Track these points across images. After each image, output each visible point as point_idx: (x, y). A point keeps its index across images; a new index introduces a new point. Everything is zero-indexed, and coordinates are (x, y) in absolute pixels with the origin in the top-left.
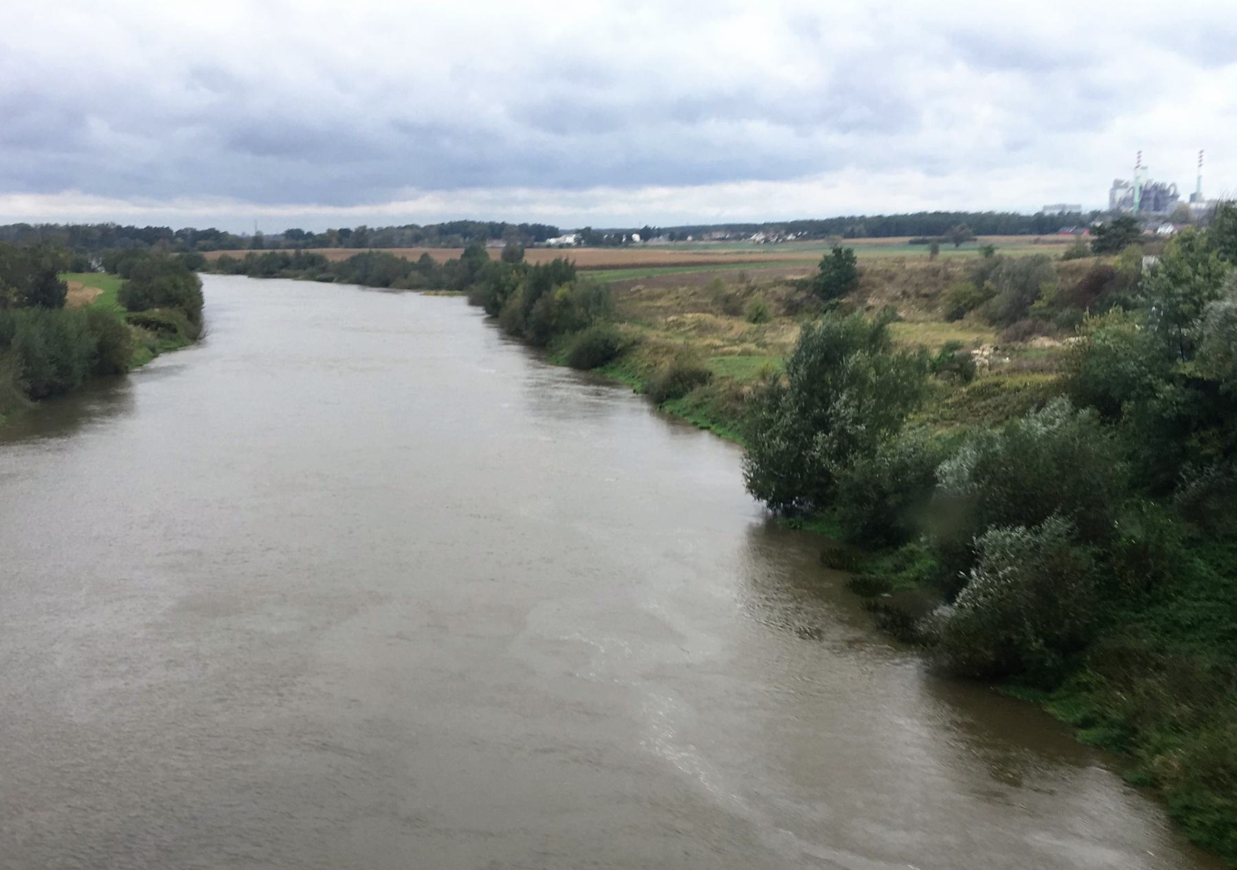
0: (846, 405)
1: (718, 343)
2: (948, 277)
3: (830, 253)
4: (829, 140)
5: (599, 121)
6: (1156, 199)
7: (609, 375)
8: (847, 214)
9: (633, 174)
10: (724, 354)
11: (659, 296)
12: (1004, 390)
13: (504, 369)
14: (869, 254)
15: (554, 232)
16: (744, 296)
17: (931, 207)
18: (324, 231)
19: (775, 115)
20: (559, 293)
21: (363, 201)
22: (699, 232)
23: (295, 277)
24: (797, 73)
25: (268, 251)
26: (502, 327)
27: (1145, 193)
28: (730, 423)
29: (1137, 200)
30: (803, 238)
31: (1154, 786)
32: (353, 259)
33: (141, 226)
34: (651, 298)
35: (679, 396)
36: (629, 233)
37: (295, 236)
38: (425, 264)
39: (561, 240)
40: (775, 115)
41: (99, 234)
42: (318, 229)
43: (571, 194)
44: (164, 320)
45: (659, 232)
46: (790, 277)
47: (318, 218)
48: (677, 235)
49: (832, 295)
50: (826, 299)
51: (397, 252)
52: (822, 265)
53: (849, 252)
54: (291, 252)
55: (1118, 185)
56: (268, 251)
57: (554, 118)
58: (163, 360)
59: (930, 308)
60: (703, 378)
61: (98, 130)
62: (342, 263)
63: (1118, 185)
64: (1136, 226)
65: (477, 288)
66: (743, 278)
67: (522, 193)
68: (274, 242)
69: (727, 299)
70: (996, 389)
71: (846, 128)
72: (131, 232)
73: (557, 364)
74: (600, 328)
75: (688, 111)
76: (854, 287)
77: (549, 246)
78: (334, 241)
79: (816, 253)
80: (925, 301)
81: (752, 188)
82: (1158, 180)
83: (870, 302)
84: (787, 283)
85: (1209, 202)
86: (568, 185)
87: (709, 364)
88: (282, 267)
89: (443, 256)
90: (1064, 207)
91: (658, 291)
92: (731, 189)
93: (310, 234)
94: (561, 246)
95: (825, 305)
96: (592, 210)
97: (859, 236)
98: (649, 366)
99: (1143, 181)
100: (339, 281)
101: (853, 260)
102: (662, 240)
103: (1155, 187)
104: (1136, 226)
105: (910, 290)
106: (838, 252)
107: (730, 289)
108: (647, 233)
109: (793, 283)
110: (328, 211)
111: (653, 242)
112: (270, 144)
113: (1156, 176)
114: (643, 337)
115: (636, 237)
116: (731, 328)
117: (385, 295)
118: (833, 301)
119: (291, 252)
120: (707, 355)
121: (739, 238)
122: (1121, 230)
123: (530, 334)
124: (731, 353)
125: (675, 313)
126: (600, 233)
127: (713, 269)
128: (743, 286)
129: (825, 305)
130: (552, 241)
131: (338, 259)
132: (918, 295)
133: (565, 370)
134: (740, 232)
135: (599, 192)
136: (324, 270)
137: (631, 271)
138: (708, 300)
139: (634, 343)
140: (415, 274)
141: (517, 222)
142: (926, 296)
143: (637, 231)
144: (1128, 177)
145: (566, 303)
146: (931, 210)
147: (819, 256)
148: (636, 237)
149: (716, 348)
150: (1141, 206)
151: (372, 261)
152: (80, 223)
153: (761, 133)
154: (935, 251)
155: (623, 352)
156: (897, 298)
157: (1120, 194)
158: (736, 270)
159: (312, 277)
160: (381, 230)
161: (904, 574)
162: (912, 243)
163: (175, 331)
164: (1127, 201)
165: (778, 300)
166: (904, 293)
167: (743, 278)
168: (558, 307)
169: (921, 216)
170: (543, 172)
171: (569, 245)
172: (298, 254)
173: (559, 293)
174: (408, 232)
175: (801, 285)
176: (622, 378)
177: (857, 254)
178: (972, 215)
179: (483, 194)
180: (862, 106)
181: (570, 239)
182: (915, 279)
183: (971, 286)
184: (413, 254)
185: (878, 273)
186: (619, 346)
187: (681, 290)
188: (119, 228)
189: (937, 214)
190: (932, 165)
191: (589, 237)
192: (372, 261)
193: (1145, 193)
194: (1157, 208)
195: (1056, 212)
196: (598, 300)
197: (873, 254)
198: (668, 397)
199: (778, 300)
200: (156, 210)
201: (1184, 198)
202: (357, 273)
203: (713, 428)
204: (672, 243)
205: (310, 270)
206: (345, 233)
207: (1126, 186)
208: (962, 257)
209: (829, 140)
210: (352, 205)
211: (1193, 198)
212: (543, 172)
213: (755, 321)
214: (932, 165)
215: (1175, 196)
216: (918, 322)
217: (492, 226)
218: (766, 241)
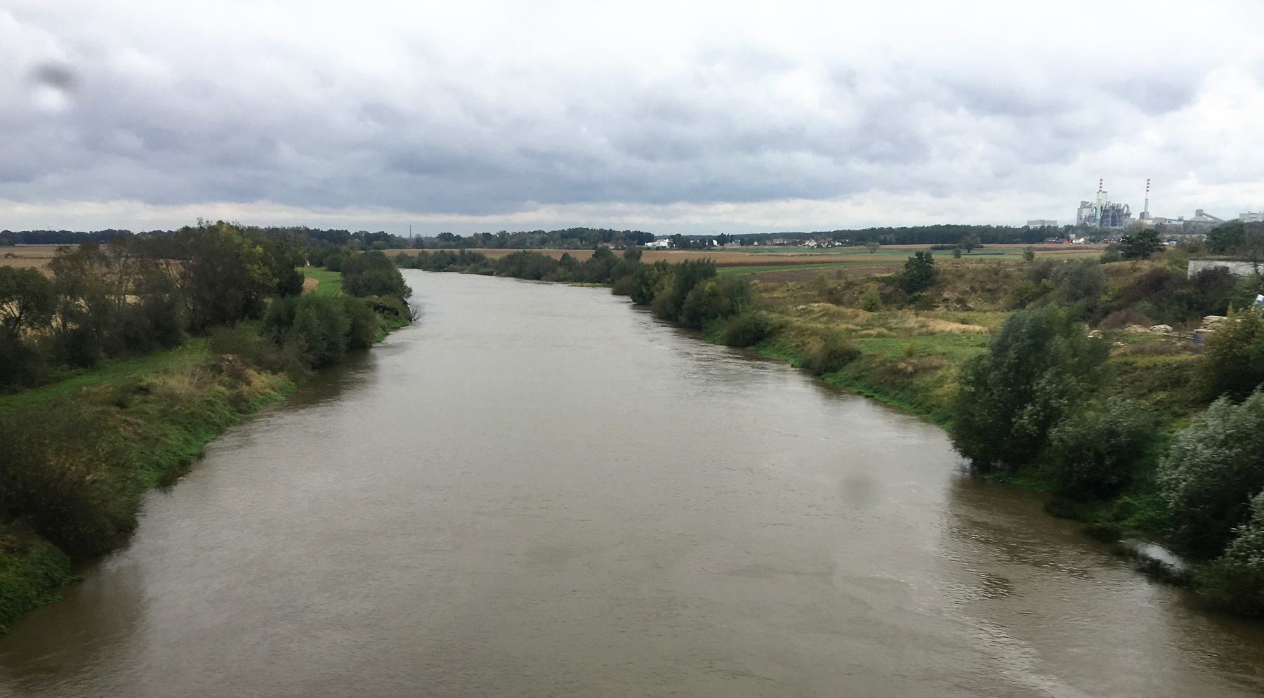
0: (1050, 383)
1: (851, 326)
2: (1007, 276)
3: (914, 256)
4: (858, 167)
5: (681, 151)
6: (1113, 217)
7: (763, 352)
9: (706, 193)
10: (863, 336)
11: (773, 289)
12: (1136, 369)
14: (942, 259)
15: (650, 238)
16: (844, 289)
17: (943, 222)
18: (471, 235)
19: (817, 147)
20: (708, 285)
22: (763, 239)
23: (461, 271)
26: (654, 312)
27: (1105, 211)
28: (893, 393)
29: (1099, 217)
30: (850, 244)
31: (165, 416)
32: (1205, 271)
33: (325, 229)
34: (766, 290)
35: (834, 370)
36: (710, 239)
37: (446, 238)
38: (567, 262)
39: (656, 243)
40: (817, 147)
42: (466, 234)
43: (658, 208)
44: (388, 305)
45: (732, 238)
46: (878, 275)
47: (465, 225)
48: (746, 240)
49: (915, 290)
50: (909, 292)
51: (545, 251)
52: (907, 266)
53: (928, 255)
54: (457, 251)
55: (1084, 205)
57: (649, 148)
58: (394, 338)
59: (993, 300)
60: (852, 356)
61: (286, 153)
63: (1084, 205)
64: (1159, 236)
65: (625, 281)
66: (840, 275)
67: (620, 206)
68: (432, 243)
69: (831, 292)
70: (1128, 368)
71: (872, 159)
72: (317, 234)
73: (714, 342)
74: (746, 316)
75: (751, 143)
76: (933, 283)
77: (649, 248)
79: (900, 256)
80: (988, 295)
81: (797, 205)
82: (1115, 202)
83: (946, 295)
84: (877, 279)
85: (1154, 219)
86: (655, 201)
87: (854, 344)
89: (583, 255)
90: (1043, 222)
91: (772, 284)
92: (782, 205)
93: (458, 237)
94: (658, 249)
95: (909, 297)
96: (673, 221)
97: (891, 243)
98: (798, 346)
99: (1104, 203)
100: (498, 274)
101: (931, 261)
102: (734, 245)
103: (1113, 207)
104: (1159, 236)
105: (977, 286)
106: (919, 254)
107: (832, 284)
108: (723, 239)
109: (883, 280)
111: (728, 246)
112: (425, 166)
114: (787, 322)
115: (715, 242)
116: (857, 316)
117: (592, 290)
118: (916, 294)
119: (457, 251)
120: (851, 337)
121: (795, 244)
122: (1146, 240)
123: (683, 319)
124: (869, 336)
125: (803, 303)
126: (688, 238)
127: (923, 266)
128: (843, 281)
129: (909, 297)
130: (649, 244)
131: (497, 258)
132: (983, 289)
133: (723, 348)
134: (796, 239)
135: (680, 206)
136: (485, 265)
137: (738, 268)
138: (814, 293)
139: (781, 327)
140: (561, 270)
141: (622, 229)
142: (989, 290)
143: (715, 238)
144: (1092, 199)
145: (713, 294)
147: (905, 258)
148: (715, 242)
149: (856, 331)
150: (1101, 222)
151: (526, 259)
153: (806, 161)
154: (958, 255)
155: (770, 334)
156: (966, 292)
157: (1086, 212)
158: (836, 268)
159: (476, 272)
160: (515, 235)
161: (1125, 522)
163: (397, 314)
164: (1091, 218)
166: (972, 288)
167: (840, 275)
168: (706, 299)
169: (937, 227)
170: (637, 191)
171: (664, 248)
172: (462, 253)
173: (708, 285)
174: (537, 236)
175: (888, 281)
176: (775, 356)
179: (590, 207)
180: (884, 141)
181: (664, 243)
182: (980, 277)
183: (1031, 283)
184: (556, 254)
185: (950, 273)
186: (769, 329)
187: (791, 284)
188: (307, 230)
190: (938, 189)
191: (679, 242)
192: (526, 259)
195: (1039, 226)
196: (739, 291)
198: (826, 371)
200: (330, 217)
201: (1135, 216)
202: (514, 268)
203: (876, 396)
204: (745, 247)
205: (473, 265)
206: (487, 236)
207: (1090, 206)
209: (858, 167)
210: (486, 214)
211: (1142, 215)
212: (637, 191)
213: (870, 310)
214: (938, 189)
215: (1128, 215)
216: (985, 312)
217: (602, 231)
218: (819, 246)
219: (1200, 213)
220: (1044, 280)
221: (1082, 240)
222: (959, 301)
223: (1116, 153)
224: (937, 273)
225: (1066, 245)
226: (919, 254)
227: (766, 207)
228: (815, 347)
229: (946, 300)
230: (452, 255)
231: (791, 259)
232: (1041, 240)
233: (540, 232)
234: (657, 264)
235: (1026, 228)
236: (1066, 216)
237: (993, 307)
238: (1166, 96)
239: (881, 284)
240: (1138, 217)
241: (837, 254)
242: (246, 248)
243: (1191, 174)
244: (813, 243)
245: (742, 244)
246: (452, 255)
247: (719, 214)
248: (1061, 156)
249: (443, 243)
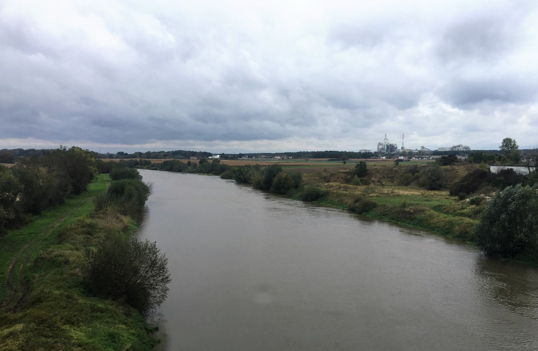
4: (289, 128)
5: (218, 119)
8: (302, 151)
13: (254, 201)
15: (210, 154)
19: (273, 119)
21: (136, 143)
24: (282, 107)
25: (130, 159)
27: (388, 146)
32: (165, 162)
40: (273, 119)
41: (52, 152)
42: (130, 152)
43: (207, 142)
48: (250, 156)
52: (356, 167)
53: (365, 163)
55: (380, 144)
56: (130, 159)
57: (204, 118)
59: (392, 181)
60: (374, 206)
62: (161, 164)
63: (380, 144)
67: (191, 142)
69: (325, 178)
71: (296, 124)
75: (247, 117)
78: (138, 156)
79: (352, 164)
80: (390, 179)
81: (265, 142)
82: (391, 143)
83: (373, 179)
86: (206, 139)
88: (135, 165)
90: (365, 150)
92: (259, 142)
93: (126, 154)
99: (387, 143)
100: (160, 170)
101: (365, 165)
105: (385, 175)
107: (324, 174)
110: (105, 146)
113: (391, 142)
119: (138, 159)
121: (271, 158)
124: (373, 196)
126: (228, 155)
130: (210, 157)
135: (217, 142)
142: (390, 177)
144: (383, 142)
146: (329, 150)
152: (46, 148)
153: (268, 124)
156: (380, 178)
157: (381, 147)
162: (329, 160)
164: (383, 149)
165: (342, 178)
170: (198, 135)
172: (141, 161)
174: (162, 154)
175: (348, 173)
177: (367, 164)
178: (37, 150)
179: (177, 142)
180: (300, 117)
189: (317, 152)
190: (320, 136)
191: (223, 156)
193: (388, 146)
194: (391, 152)
197: (373, 163)
199: (342, 178)
201: (399, 148)
203: (399, 223)
205: (147, 166)
208: (332, 165)
209: (289, 128)
210: (132, 144)
212: (198, 135)
214: (320, 136)
215: (396, 148)
219: (423, 147)
220: (416, 174)
221: (384, 158)
222: (379, 182)
223: (388, 124)
224: (368, 170)
225: (378, 159)
226: (361, 162)
227: (252, 143)
228: (350, 201)
229: (373, 181)
230: (175, 163)
231: (292, 164)
232: (369, 158)
233: (163, 152)
234: (246, 166)
235: (360, 152)
236: (373, 148)
237: (393, 184)
238: (406, 102)
239: (346, 175)
240: (400, 149)
241: (292, 162)
242: (89, 159)
243: (415, 133)
244: (279, 158)
245: (249, 157)
246: (175, 163)
247: (233, 145)
248: (367, 125)
249: (120, 156)
